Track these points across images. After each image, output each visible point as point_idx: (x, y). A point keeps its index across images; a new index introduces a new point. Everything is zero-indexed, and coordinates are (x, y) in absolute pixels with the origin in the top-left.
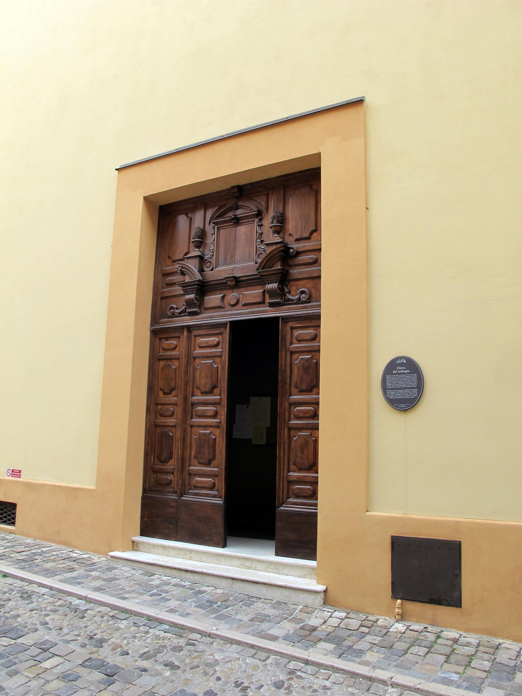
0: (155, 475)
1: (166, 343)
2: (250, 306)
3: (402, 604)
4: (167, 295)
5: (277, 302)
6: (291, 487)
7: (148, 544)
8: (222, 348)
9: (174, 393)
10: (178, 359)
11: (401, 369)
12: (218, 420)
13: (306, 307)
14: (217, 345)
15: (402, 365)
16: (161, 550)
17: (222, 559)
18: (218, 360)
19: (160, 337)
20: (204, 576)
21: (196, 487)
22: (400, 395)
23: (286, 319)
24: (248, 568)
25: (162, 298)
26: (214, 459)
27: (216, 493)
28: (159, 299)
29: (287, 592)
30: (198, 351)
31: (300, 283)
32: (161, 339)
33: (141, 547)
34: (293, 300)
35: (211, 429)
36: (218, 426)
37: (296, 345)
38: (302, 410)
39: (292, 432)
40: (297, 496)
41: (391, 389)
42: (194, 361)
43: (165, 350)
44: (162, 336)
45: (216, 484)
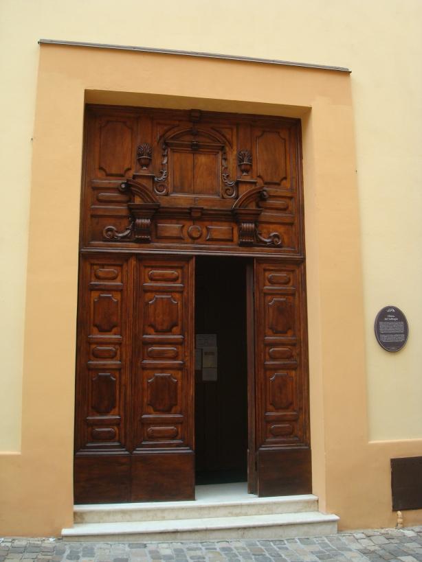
0: (90, 429)
1: (102, 272)
2: (220, 243)
3: (403, 515)
4: (100, 213)
5: (248, 242)
6: (269, 427)
7: (91, 512)
8: (293, 286)
9: (114, 330)
10: (121, 291)
11: (391, 317)
12: (181, 362)
13: (280, 252)
14: (175, 280)
15: (391, 313)
16: (119, 516)
17: (206, 512)
18: (177, 296)
19: (147, 265)
20: (208, 532)
21: (151, 438)
22: (391, 339)
23: (260, 260)
24: (237, 515)
25: (92, 216)
26: (176, 405)
27: (180, 442)
28: (89, 217)
29: (305, 528)
30: (149, 284)
31: (272, 226)
32: (92, 265)
33: (87, 518)
34: (266, 243)
35: (171, 372)
36: (181, 368)
37: (268, 287)
38: (279, 351)
39: (268, 373)
40: (275, 436)
41: (384, 334)
42: (264, 297)
43: (98, 278)
44: (93, 261)
45: (180, 433)
